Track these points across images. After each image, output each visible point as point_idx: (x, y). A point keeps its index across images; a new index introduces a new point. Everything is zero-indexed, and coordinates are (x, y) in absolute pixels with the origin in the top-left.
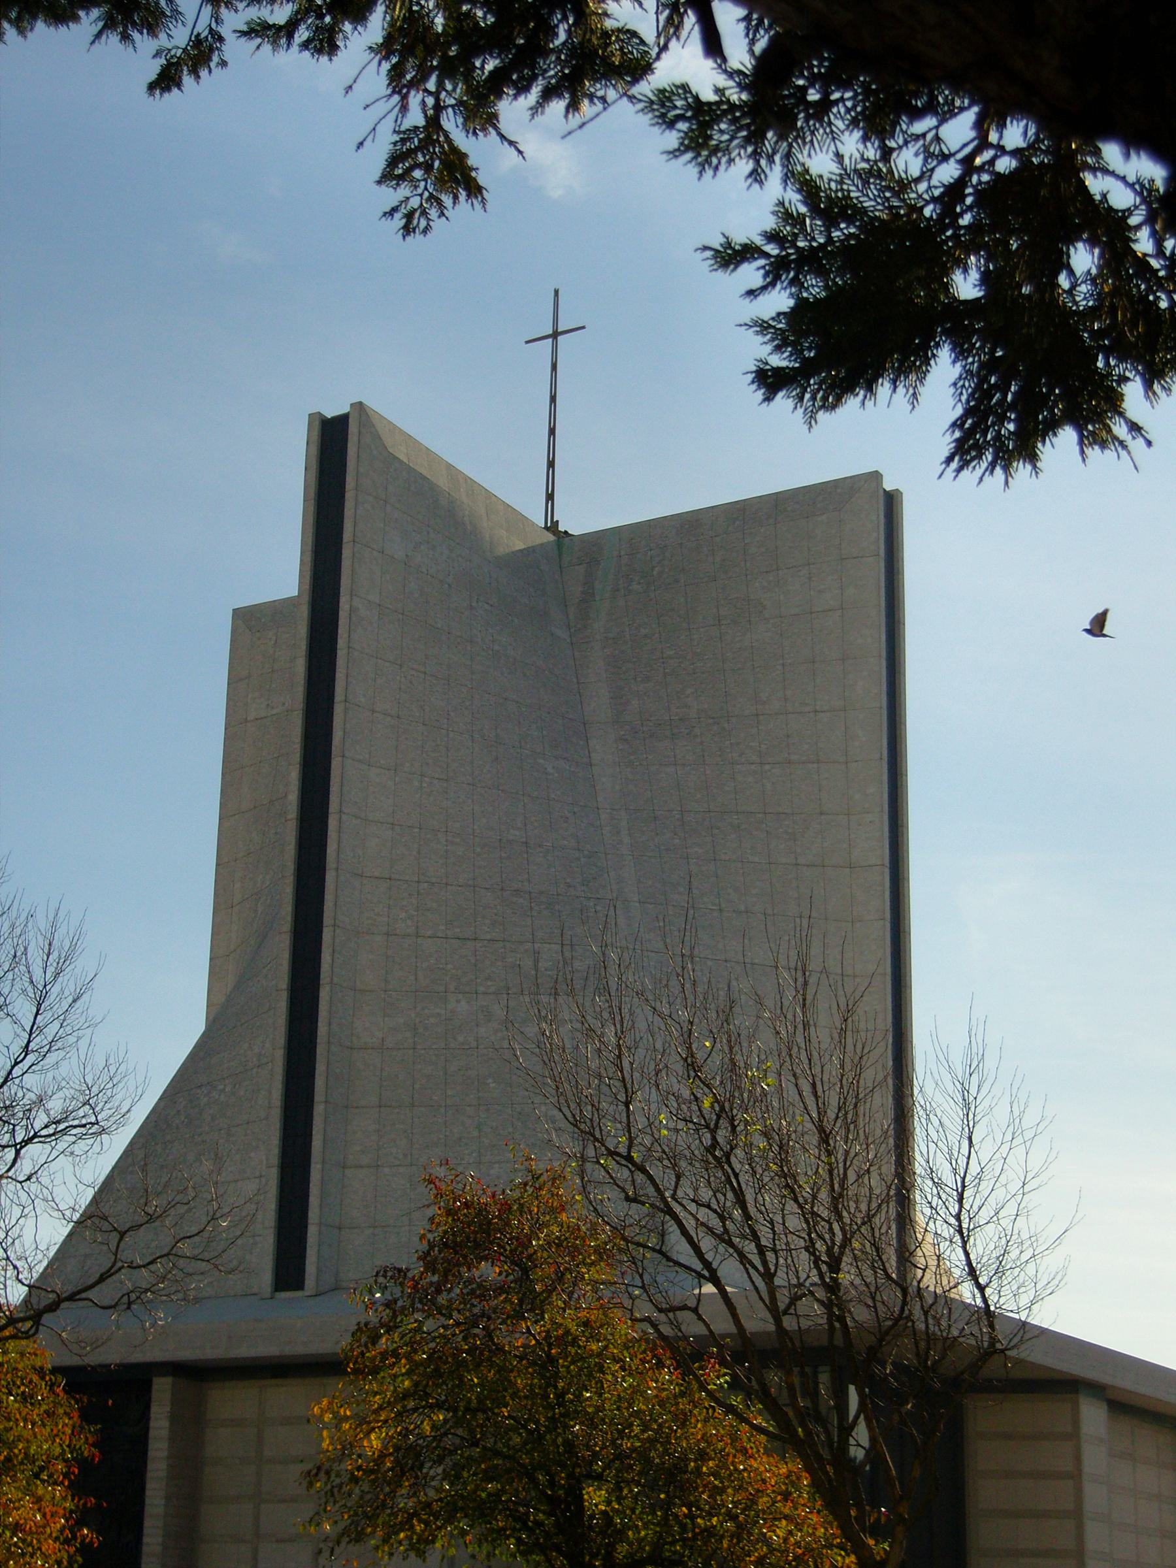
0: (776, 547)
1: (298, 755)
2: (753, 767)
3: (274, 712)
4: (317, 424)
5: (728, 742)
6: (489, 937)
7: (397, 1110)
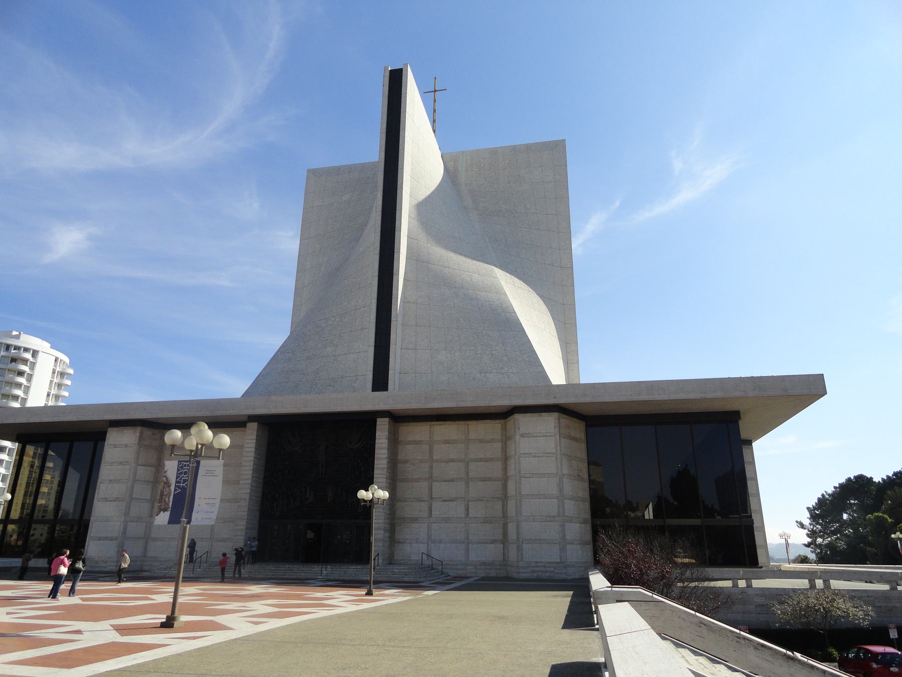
3: (325, 204)
4: (388, 74)
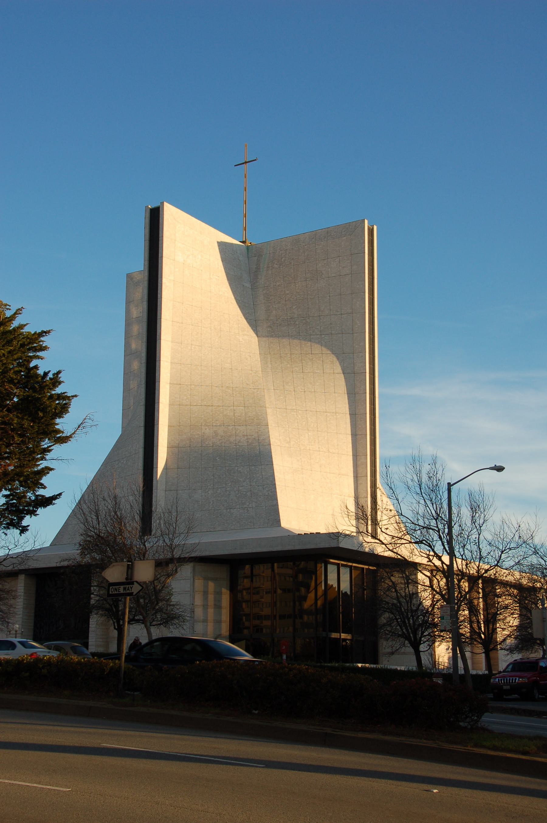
0: (327, 250)
1: (145, 339)
2: (318, 336)
4: (148, 211)
5: (309, 327)
6: (217, 405)
7: (184, 470)
